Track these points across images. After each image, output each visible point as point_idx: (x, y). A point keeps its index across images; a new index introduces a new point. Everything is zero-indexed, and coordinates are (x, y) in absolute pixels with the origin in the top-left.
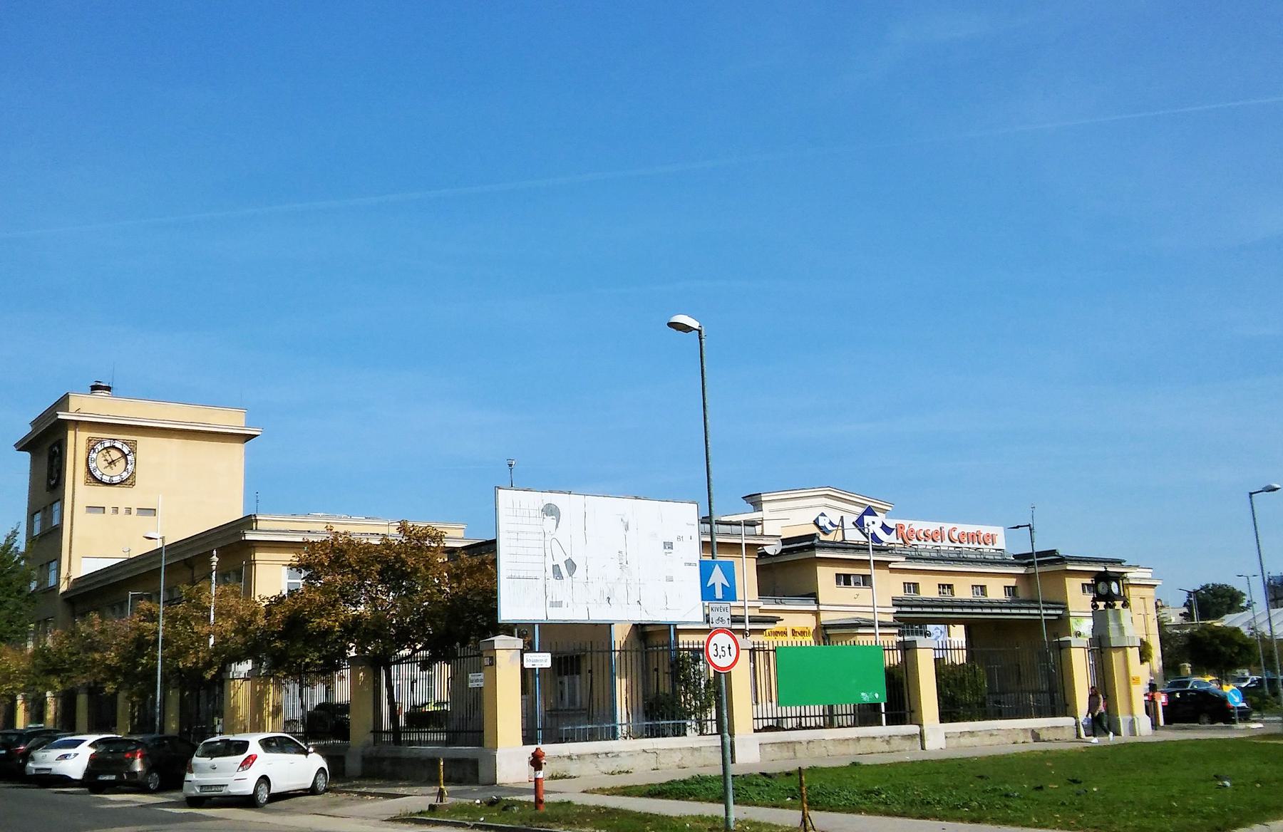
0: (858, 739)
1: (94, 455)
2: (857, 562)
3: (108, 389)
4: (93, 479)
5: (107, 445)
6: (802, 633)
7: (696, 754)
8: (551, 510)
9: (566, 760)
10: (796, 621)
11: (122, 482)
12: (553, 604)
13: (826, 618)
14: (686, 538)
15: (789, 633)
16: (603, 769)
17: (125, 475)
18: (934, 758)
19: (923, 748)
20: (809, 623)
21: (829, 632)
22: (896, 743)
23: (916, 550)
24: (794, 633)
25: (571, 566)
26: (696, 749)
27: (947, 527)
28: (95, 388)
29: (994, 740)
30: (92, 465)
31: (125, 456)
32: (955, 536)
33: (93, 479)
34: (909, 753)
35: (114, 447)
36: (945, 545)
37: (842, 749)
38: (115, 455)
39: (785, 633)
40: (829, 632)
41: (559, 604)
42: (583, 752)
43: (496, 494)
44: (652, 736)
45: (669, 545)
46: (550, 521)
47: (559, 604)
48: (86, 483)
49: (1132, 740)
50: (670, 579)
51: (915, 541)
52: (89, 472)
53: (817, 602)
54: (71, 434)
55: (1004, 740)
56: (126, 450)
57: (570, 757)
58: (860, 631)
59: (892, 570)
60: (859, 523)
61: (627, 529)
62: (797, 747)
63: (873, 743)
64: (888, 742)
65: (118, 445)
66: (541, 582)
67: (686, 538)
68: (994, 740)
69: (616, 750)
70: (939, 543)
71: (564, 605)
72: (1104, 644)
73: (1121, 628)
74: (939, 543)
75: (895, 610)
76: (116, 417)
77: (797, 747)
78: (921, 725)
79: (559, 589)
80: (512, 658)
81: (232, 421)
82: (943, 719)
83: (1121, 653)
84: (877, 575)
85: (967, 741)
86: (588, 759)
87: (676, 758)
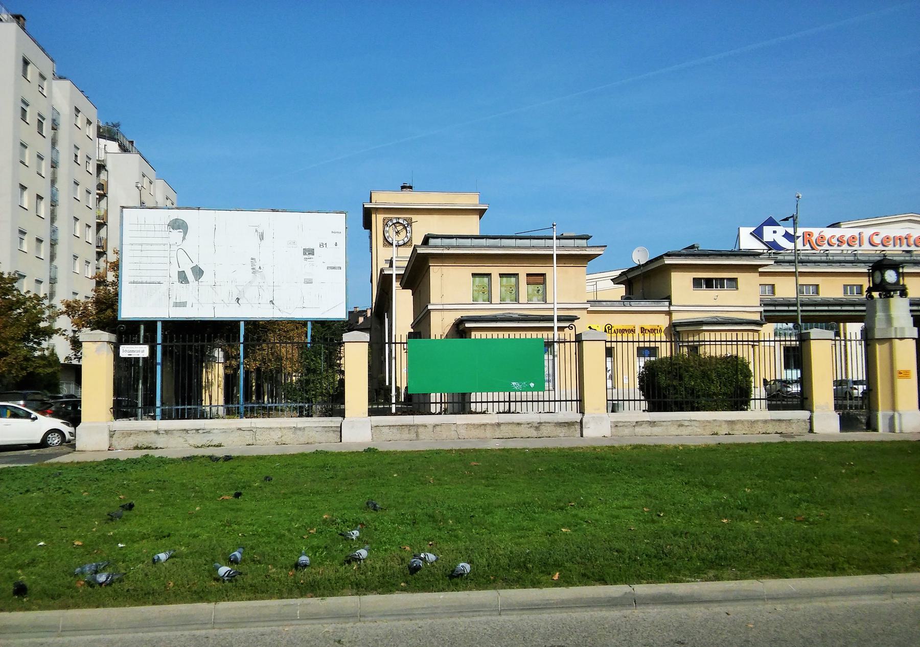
0: (499, 425)
1: (387, 229)
3: (411, 187)
6: (653, 331)
7: (299, 433)
8: (178, 225)
9: (153, 435)
11: (404, 244)
12: (176, 305)
13: (677, 318)
14: (331, 244)
15: (638, 331)
16: (192, 442)
17: (406, 240)
18: (820, 440)
19: (582, 436)
20: (663, 322)
21: (678, 329)
22: (545, 431)
24: (643, 330)
25: (198, 272)
26: (300, 429)
27: (867, 232)
28: (403, 187)
29: (684, 431)
30: (387, 235)
31: (405, 228)
32: (877, 240)
34: (328, 443)
38: (400, 228)
39: (633, 331)
40: (678, 329)
41: (184, 304)
42: (173, 428)
43: (122, 211)
45: (309, 252)
46: (177, 235)
47: (184, 304)
48: (384, 245)
49: (890, 437)
50: (309, 282)
51: (826, 247)
52: (385, 239)
53: (670, 304)
54: (373, 216)
56: (405, 223)
57: (157, 432)
58: (704, 328)
59: (763, 274)
61: (262, 237)
62: (421, 430)
63: (517, 428)
64: (537, 428)
65: (401, 221)
67: (331, 244)
68: (684, 431)
70: (856, 247)
72: (870, 337)
73: (889, 320)
74: (856, 247)
75: (762, 309)
77: (421, 430)
78: (811, 411)
79: (182, 292)
80: (98, 350)
81: (470, 200)
82: (372, 412)
83: (886, 346)
87: (276, 436)
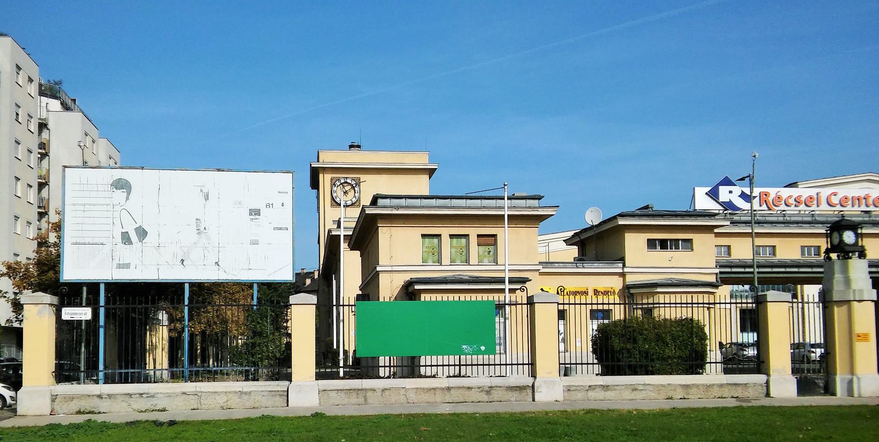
0: (449, 389)
2: (673, 228)
3: (359, 147)
4: (335, 203)
5: (342, 181)
6: (606, 293)
8: (121, 185)
9: (96, 399)
10: (602, 281)
11: (352, 205)
12: (120, 266)
13: (631, 279)
15: (591, 293)
16: (135, 406)
17: (354, 200)
19: (534, 400)
20: (617, 284)
21: (632, 291)
22: (496, 395)
23: (784, 216)
24: (596, 292)
25: (142, 233)
26: (246, 393)
27: (825, 192)
28: (351, 147)
30: (335, 195)
31: (353, 188)
32: (835, 200)
33: (335, 203)
35: (346, 182)
36: (792, 210)
37: (429, 397)
38: (348, 188)
39: (586, 293)
40: (632, 291)
44: (277, 380)
46: (120, 195)
48: (332, 206)
50: (255, 243)
52: (333, 199)
53: (624, 266)
54: (321, 176)
55: (653, 395)
58: (659, 290)
59: (718, 235)
60: (713, 194)
61: (207, 197)
62: (369, 394)
63: (467, 393)
65: (349, 181)
66: (107, 249)
67: (277, 204)
69: (152, 391)
70: (814, 208)
71: (132, 266)
73: (847, 282)
74: (814, 208)
75: (717, 271)
76: (343, 163)
77: (369, 394)
78: (768, 375)
79: (126, 253)
81: (420, 160)
82: (319, 376)
83: (844, 308)
84: (698, 239)
85: (600, 394)
86: (122, 398)
87: (221, 400)
